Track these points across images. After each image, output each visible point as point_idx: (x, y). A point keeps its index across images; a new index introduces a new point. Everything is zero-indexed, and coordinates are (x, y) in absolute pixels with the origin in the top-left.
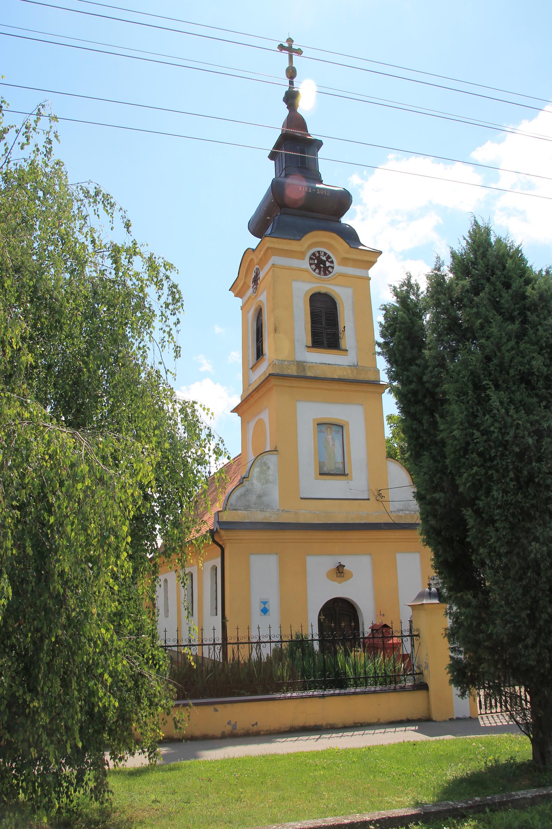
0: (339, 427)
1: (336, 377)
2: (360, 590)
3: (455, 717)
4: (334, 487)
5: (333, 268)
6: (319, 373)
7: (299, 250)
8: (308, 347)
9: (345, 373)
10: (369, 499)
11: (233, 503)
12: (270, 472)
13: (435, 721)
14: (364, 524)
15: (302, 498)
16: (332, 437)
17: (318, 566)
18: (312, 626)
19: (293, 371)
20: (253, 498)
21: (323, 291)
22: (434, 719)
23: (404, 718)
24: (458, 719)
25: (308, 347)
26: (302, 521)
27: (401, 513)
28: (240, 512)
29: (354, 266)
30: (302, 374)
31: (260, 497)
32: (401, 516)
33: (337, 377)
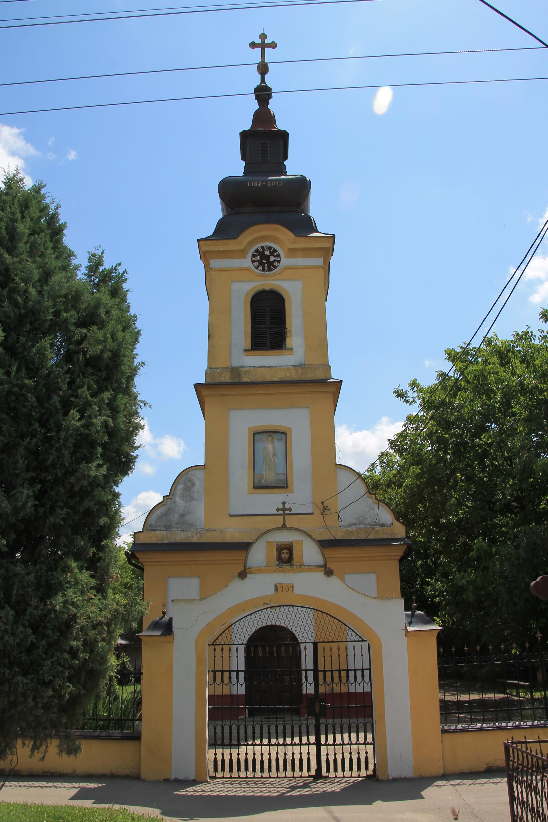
1: (276, 379)
3: (172, 778)
5: (279, 262)
6: (257, 377)
7: (237, 249)
8: (245, 350)
9: (288, 374)
10: (312, 514)
11: (153, 523)
12: (195, 488)
13: (144, 780)
15: (230, 516)
16: (271, 447)
19: (226, 378)
20: (175, 517)
21: (267, 288)
22: (143, 776)
23: (107, 771)
24: (395, 780)
25: (245, 350)
26: (228, 540)
27: (353, 528)
28: (158, 532)
31: (182, 516)
32: (352, 532)
33: (277, 380)
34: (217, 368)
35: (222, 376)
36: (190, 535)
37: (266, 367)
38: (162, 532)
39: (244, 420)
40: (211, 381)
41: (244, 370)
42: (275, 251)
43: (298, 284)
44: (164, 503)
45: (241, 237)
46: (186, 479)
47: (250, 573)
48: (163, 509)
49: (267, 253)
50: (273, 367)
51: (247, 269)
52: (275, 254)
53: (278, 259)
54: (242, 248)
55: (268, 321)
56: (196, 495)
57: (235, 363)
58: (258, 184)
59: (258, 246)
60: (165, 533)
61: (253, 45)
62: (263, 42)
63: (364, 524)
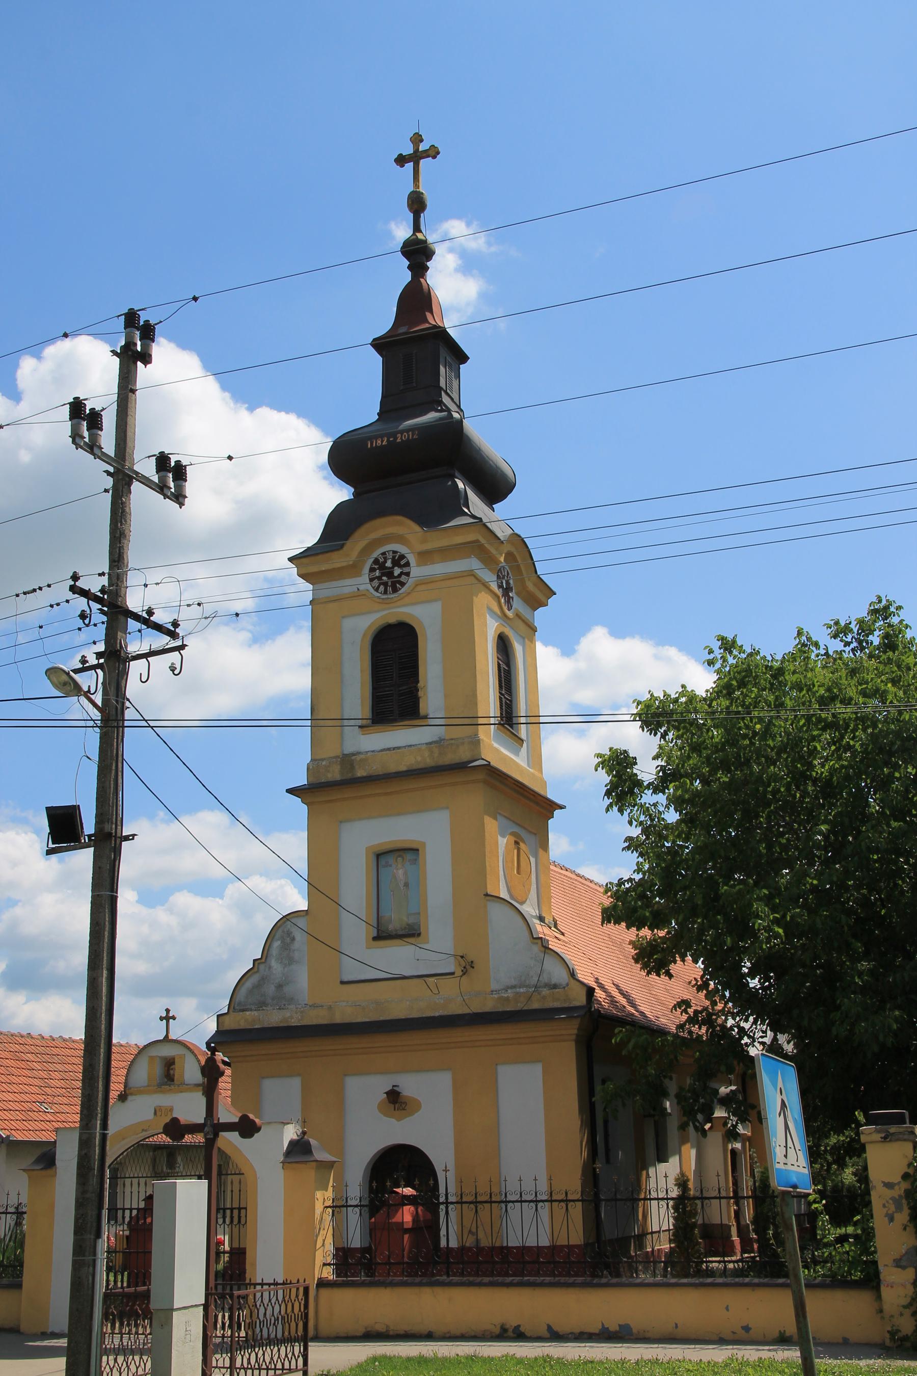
0: (409, 852)
1: (403, 768)
2: (432, 1132)
4: (398, 958)
5: (408, 574)
6: (375, 768)
7: (344, 564)
9: (419, 759)
12: (296, 945)
13: (22, 1334)
14: (441, 1017)
15: (342, 983)
17: (364, 1091)
18: (666, 1176)
19: (335, 774)
20: (270, 989)
21: (392, 620)
26: (338, 1019)
27: (510, 994)
28: (248, 1013)
29: (444, 560)
30: (349, 776)
31: (280, 987)
32: (507, 999)
34: (323, 760)
35: (329, 772)
36: (288, 1014)
37: (389, 749)
38: (253, 1013)
39: (365, 834)
41: (358, 758)
42: (402, 557)
43: (436, 608)
44: (256, 969)
45: (349, 544)
46: (283, 932)
47: (131, 1094)
48: (254, 979)
49: (389, 564)
50: (399, 748)
51: (359, 595)
52: (402, 562)
53: (406, 570)
54: (351, 563)
55: (394, 672)
57: (349, 748)
58: (382, 441)
59: (376, 554)
60: (256, 1013)
61: (401, 160)
62: (416, 151)
63: (528, 986)
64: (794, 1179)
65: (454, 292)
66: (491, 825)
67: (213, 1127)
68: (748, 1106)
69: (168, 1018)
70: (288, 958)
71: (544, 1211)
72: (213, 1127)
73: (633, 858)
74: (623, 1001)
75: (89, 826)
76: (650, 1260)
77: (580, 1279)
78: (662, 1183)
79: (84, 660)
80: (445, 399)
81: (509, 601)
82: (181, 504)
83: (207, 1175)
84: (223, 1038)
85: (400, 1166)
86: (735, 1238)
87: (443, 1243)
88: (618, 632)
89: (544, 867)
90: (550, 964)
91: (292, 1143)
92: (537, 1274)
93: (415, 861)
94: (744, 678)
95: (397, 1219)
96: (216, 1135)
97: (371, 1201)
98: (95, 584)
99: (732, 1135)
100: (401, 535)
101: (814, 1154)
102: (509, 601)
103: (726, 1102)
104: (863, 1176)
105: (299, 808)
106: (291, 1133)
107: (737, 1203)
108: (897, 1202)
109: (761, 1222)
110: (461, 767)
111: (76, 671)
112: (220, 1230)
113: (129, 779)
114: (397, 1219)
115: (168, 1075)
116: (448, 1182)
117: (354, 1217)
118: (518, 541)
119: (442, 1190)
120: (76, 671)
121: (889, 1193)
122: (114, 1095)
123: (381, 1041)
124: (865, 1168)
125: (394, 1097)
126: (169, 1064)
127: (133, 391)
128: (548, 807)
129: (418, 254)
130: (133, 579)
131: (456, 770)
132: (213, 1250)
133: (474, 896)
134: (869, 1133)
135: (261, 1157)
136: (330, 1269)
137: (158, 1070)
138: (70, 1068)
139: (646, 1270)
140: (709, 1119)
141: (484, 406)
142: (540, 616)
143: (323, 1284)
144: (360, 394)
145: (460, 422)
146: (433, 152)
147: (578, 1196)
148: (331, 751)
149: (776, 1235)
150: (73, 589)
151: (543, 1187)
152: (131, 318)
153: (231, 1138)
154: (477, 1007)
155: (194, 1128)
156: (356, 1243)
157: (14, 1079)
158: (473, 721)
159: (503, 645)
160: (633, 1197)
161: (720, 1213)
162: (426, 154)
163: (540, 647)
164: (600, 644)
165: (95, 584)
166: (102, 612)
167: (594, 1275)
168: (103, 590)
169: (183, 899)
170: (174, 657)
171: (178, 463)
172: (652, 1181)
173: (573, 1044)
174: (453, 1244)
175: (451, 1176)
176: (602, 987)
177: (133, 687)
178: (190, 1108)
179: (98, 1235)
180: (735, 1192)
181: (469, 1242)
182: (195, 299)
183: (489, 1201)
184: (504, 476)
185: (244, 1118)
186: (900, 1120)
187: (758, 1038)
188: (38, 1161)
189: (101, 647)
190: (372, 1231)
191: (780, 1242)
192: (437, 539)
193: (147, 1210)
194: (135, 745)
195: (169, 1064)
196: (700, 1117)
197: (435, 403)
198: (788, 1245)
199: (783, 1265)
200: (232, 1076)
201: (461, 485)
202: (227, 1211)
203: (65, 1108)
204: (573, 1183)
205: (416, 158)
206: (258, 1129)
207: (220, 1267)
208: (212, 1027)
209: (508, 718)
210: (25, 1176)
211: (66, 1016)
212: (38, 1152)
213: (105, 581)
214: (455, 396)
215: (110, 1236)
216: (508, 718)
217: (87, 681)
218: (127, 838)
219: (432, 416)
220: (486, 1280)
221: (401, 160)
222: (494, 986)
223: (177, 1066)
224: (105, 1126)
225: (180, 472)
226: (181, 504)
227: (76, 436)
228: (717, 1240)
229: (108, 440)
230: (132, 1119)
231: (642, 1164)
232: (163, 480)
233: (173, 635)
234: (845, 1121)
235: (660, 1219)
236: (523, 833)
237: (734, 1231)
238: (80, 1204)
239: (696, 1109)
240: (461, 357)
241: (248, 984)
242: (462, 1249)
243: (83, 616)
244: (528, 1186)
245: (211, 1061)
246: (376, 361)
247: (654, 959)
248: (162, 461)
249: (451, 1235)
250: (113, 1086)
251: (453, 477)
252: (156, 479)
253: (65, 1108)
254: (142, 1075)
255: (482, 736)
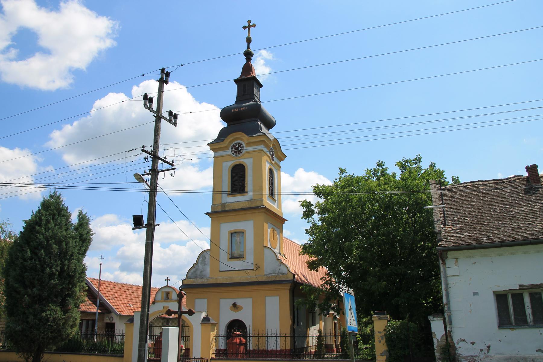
0: (241, 233)
2: (246, 316)
4: (237, 264)
5: (243, 150)
6: (231, 207)
12: (206, 260)
17: (226, 303)
19: (219, 209)
20: (198, 273)
21: (238, 163)
26: (218, 282)
27: (270, 276)
31: (201, 272)
39: (227, 227)
40: (213, 211)
42: (241, 144)
43: (251, 160)
49: (237, 146)
51: (229, 155)
55: (238, 179)
56: (206, 263)
61: (244, 28)
62: (249, 25)
64: (353, 329)
65: (260, 70)
66: (266, 225)
67: (180, 312)
68: (340, 310)
69: (167, 280)
70: (204, 264)
71: (279, 339)
72: (180, 312)
73: (308, 236)
74: (304, 279)
75: (145, 222)
76: (309, 354)
77: (288, 359)
78: (314, 332)
79: (145, 172)
80: (255, 98)
81: (273, 158)
82: (176, 126)
83: (179, 326)
84: (184, 287)
85: (236, 326)
86: (334, 348)
87: (248, 348)
88: (307, 170)
89: (281, 238)
90: (282, 267)
91: (204, 318)
92: (276, 357)
93: (243, 236)
94: (349, 184)
95: (235, 341)
96: (181, 315)
97: (227, 335)
98: (149, 149)
99: (335, 318)
100: (242, 138)
101: (359, 324)
102: (273, 158)
103: (333, 309)
104: (372, 331)
105: (208, 219)
106: (204, 315)
107: (335, 338)
108: (382, 337)
109: (342, 343)
110: (257, 208)
111: (143, 175)
112: (182, 343)
113: (158, 208)
114: (235, 341)
115: (167, 296)
116: (250, 331)
117: (222, 340)
118: (276, 140)
119: (248, 333)
120: (143, 175)
121: (380, 335)
122: (151, 302)
123: (230, 289)
124: (373, 327)
125: (235, 305)
126: (168, 293)
127: (163, 92)
128: (283, 220)
129: (248, 55)
130: (160, 148)
131: (256, 209)
132: (180, 349)
133: (260, 246)
134: (374, 317)
135: (195, 322)
136: (215, 355)
137: (164, 295)
138: (138, 294)
139: (308, 356)
140: (328, 313)
141: (268, 101)
142: (282, 163)
143: (212, 359)
144: (230, 96)
145: (260, 105)
146: (254, 26)
147: (289, 335)
148: (218, 202)
149: (347, 347)
150: (143, 150)
151: (278, 332)
152: (163, 70)
153: (186, 315)
154: (260, 279)
155: (175, 313)
156: (222, 348)
157: (121, 297)
158: (261, 193)
159: (271, 172)
160: (305, 336)
161: (330, 341)
162: (252, 26)
163: (282, 174)
164: (301, 173)
165: (149, 149)
166: (151, 157)
167: (293, 358)
168: (151, 151)
169: (173, 246)
170: (172, 171)
171: (175, 114)
172: (311, 331)
173: (288, 291)
174: (251, 349)
175: (251, 328)
176: (297, 275)
177: (160, 181)
178: (174, 307)
179: (146, 342)
180: (335, 334)
181: (256, 348)
182: (182, 65)
183: (262, 336)
184: (272, 121)
185: (190, 310)
186: (384, 313)
187: (343, 290)
188: (128, 321)
189: (150, 168)
190: (227, 344)
191: (348, 349)
192: (252, 140)
193: (161, 336)
194: (159, 196)
195: (168, 293)
196: (325, 312)
197: (252, 99)
198: (350, 348)
199: (348, 355)
200: (186, 298)
201: (259, 123)
202: (184, 337)
203: (137, 306)
204: (287, 331)
205: (249, 27)
206: (194, 313)
207: (182, 354)
208: (181, 284)
209: (272, 193)
210: (124, 325)
211: (137, 279)
212: (129, 318)
213: (152, 148)
214: (258, 97)
215: (149, 343)
216: (272, 193)
217: (146, 177)
218: (156, 225)
219: (251, 103)
220: (261, 359)
221: (244, 28)
222: (265, 273)
223: (170, 294)
224: (148, 311)
225: (176, 116)
226: (176, 126)
227: (145, 105)
228: (329, 348)
229: (154, 106)
230: (156, 309)
231: (308, 326)
232: (170, 119)
233: (172, 165)
234: (369, 314)
235: (313, 342)
236: (275, 228)
237: (334, 346)
238: (141, 333)
239: (325, 309)
240: (261, 86)
241: (192, 271)
242: (254, 350)
243: (145, 158)
244: (274, 332)
245: (180, 293)
246: (235, 86)
247: (313, 266)
248: (170, 113)
249: (251, 347)
250: (151, 300)
251: (257, 121)
252: (168, 118)
253: (137, 306)
254: (159, 297)
255: (264, 199)
